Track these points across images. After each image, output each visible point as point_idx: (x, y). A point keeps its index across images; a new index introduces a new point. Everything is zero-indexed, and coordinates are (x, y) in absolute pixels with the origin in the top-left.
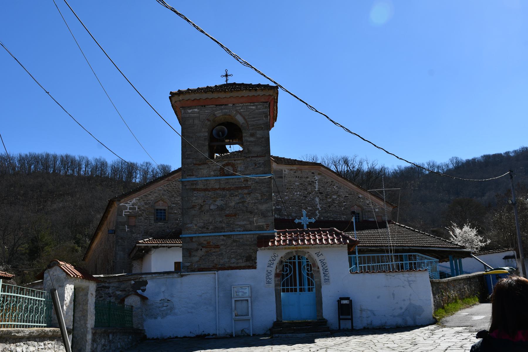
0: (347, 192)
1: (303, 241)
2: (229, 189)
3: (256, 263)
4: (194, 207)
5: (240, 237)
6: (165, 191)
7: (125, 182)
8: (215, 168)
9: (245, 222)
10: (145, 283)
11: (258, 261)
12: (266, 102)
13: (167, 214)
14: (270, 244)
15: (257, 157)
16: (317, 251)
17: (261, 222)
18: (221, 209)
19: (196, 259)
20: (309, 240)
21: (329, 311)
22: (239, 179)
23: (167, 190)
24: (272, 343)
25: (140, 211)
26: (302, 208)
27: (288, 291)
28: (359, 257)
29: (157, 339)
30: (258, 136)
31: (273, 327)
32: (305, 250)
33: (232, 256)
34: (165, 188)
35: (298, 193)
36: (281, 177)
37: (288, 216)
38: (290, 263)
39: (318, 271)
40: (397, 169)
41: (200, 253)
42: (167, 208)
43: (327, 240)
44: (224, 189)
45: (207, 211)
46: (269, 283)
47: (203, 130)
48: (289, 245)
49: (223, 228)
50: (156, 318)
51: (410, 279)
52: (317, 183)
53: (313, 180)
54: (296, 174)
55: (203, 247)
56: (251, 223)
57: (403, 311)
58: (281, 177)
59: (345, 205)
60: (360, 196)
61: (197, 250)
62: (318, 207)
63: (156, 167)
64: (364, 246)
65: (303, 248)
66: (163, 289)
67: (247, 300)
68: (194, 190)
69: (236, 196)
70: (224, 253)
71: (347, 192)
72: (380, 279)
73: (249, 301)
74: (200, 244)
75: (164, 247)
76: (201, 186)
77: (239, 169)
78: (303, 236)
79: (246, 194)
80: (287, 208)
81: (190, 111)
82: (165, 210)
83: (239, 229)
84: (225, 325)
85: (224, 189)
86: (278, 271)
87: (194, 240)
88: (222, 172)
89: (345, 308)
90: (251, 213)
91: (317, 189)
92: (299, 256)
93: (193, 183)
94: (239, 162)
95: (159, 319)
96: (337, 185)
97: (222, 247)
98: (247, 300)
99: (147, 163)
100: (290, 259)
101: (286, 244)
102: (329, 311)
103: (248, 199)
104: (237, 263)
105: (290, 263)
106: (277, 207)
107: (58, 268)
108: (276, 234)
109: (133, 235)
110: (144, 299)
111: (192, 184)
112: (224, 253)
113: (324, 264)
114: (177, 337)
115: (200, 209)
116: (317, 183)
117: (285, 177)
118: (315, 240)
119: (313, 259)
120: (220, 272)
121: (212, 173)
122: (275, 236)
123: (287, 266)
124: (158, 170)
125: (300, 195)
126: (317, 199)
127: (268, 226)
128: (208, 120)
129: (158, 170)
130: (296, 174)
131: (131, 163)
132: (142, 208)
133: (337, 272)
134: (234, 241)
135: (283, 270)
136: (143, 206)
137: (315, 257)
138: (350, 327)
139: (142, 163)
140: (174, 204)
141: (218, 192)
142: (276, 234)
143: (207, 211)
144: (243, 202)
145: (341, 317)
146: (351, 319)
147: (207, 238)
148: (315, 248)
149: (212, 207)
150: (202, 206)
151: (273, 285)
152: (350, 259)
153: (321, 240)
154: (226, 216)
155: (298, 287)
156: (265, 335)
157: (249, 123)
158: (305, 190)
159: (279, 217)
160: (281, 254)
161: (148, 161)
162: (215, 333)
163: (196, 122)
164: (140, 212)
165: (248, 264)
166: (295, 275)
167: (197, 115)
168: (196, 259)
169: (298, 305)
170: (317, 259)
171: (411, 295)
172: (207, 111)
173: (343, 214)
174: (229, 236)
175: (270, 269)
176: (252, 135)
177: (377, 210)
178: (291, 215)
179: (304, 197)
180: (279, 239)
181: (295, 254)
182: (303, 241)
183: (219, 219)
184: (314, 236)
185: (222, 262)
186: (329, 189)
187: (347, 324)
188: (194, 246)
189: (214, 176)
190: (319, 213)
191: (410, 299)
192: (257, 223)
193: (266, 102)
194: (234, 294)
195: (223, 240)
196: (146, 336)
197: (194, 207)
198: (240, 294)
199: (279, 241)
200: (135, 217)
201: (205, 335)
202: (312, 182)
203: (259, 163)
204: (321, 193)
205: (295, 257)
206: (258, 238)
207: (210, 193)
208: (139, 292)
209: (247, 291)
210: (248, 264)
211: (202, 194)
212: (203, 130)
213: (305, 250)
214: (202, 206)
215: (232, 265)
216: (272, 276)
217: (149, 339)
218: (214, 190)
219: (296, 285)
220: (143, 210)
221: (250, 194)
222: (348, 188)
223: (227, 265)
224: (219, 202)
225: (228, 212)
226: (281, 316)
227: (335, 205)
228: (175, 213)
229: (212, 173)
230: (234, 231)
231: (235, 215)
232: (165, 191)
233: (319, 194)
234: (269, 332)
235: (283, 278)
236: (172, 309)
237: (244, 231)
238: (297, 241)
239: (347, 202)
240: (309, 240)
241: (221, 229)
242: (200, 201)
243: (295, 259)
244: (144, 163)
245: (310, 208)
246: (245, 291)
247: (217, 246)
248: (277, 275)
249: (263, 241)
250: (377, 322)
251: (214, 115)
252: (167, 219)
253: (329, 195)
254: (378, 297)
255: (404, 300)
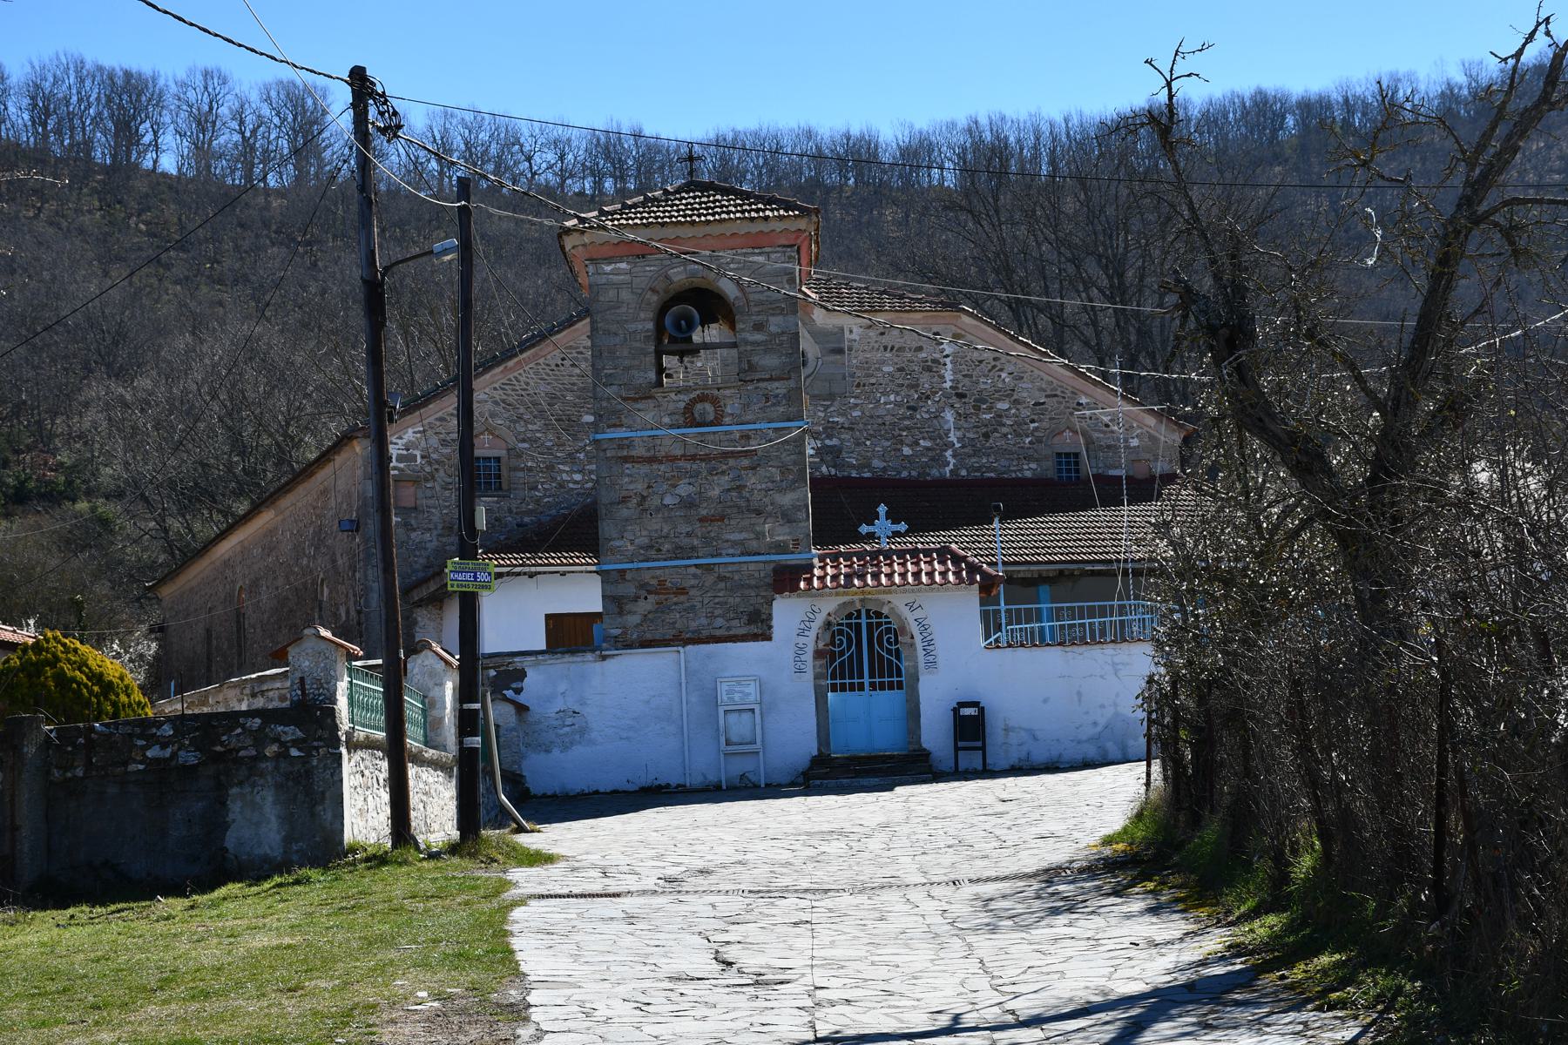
0: (1041, 390)
1: (876, 576)
2: (706, 458)
3: (770, 627)
4: (624, 500)
5: (735, 568)
6: (496, 403)
7: (105, 169)
8: (671, 407)
9: (744, 535)
10: (521, 675)
11: (774, 623)
12: (792, 246)
13: (504, 472)
14: (802, 585)
15: (771, 379)
16: (909, 598)
17: (783, 535)
18: (688, 504)
19: (633, 619)
20: (890, 576)
21: (935, 733)
22: (731, 433)
23: (504, 401)
24: (808, 792)
25: (430, 463)
26: (902, 442)
27: (843, 689)
28: (1007, 611)
29: (554, 796)
30: (773, 329)
31: (811, 768)
32: (881, 597)
33: (717, 612)
34: (498, 395)
35: (892, 397)
36: (840, 351)
37: (859, 468)
38: (849, 626)
39: (912, 645)
40: (1460, 78)
41: (644, 606)
42: (504, 452)
43: (930, 574)
44: (693, 458)
45: (658, 510)
46: (800, 671)
47: (642, 315)
48: (845, 587)
49: (693, 548)
50: (548, 751)
51: (1116, 660)
52: (949, 366)
53: (937, 356)
54: (885, 340)
55: (650, 592)
56: (759, 536)
57: (1099, 729)
58: (840, 351)
59: (1036, 429)
60: (1084, 400)
61: (636, 599)
62: (953, 438)
63: (254, 97)
64: (1073, 562)
65: (879, 592)
66: (562, 687)
67: (753, 710)
68: (626, 459)
69: (723, 473)
70: (699, 605)
71: (1041, 390)
72: (1051, 659)
73: (757, 712)
74: (643, 586)
75: (519, 574)
76: (639, 451)
77: (729, 410)
78: (877, 565)
79: (745, 469)
80: (858, 444)
81: (608, 268)
82: (498, 459)
83: (731, 551)
84: (704, 764)
85: (693, 458)
86: (821, 645)
87: (628, 576)
88: (690, 418)
89: (970, 726)
90: (759, 513)
91: (948, 385)
92: (868, 611)
93: (623, 444)
94: (728, 392)
95: (556, 752)
96: (1011, 368)
97: (692, 592)
98: (753, 710)
99: (207, 74)
100: (849, 616)
101: (839, 585)
102: (935, 733)
103: (751, 480)
104: (729, 629)
105: (849, 626)
106: (828, 442)
107: (430, 654)
108: (816, 561)
109: (413, 535)
110: (521, 709)
111: (620, 447)
112: (699, 605)
113: (924, 628)
114: (597, 792)
115: (639, 504)
116: (949, 366)
117: (850, 349)
118: (903, 575)
119: (899, 617)
120: (689, 647)
121: (666, 420)
122: (812, 566)
123: (841, 632)
124: (266, 111)
125: (896, 404)
126: (949, 416)
127: (797, 542)
128: (653, 290)
129: (266, 111)
130: (885, 340)
131: (128, 75)
132: (434, 456)
133: (956, 650)
134: (721, 578)
135: (833, 643)
136: (436, 450)
137: (905, 612)
138: (980, 768)
139: (182, 75)
140: (524, 441)
141: (681, 464)
142: (816, 561)
143: (658, 510)
144: (740, 488)
145: (960, 744)
146: (983, 749)
147: (658, 572)
148: (905, 592)
149: (668, 500)
150: (644, 498)
151: (809, 676)
152: (985, 616)
153: (917, 575)
154: (700, 520)
155: (866, 680)
156: (792, 784)
157: (751, 297)
158: (911, 386)
159: (833, 471)
160: (828, 606)
161: (210, 63)
162: (681, 782)
163: (625, 295)
164: (428, 469)
165: (754, 629)
166: (865, 652)
167: (627, 277)
168: (633, 619)
169: (867, 717)
170: (910, 617)
171: (1117, 695)
172: (650, 268)
173: (1029, 458)
174: (708, 568)
175: (802, 640)
176: (759, 327)
177: (1135, 443)
178: (868, 466)
179: (909, 408)
180: (823, 571)
181: (858, 606)
182: (876, 576)
183: (684, 528)
184: (904, 565)
185: (693, 625)
186: (985, 384)
187: (972, 760)
188: (629, 589)
189: (671, 427)
190: (954, 456)
191: (1115, 705)
192: (771, 536)
193: (792, 246)
194: (723, 696)
195: (695, 576)
196: (528, 789)
197: (624, 500)
198: (737, 697)
199: (822, 579)
200: (416, 481)
201: (660, 787)
202: (935, 361)
203: (776, 396)
204: (961, 396)
205: (859, 612)
206: (775, 571)
207: (662, 467)
208: (509, 693)
209: (752, 689)
210: (754, 629)
211: (644, 469)
212: (642, 315)
213: (881, 597)
214: (644, 498)
215: (718, 633)
216: (808, 656)
217: (535, 796)
218: (672, 459)
219: (861, 676)
220: (438, 462)
221: (754, 468)
222: (1046, 377)
223: (705, 633)
224: (684, 489)
225: (704, 512)
226: (828, 744)
227: (1005, 430)
228: (530, 469)
229: (666, 420)
230: (720, 555)
231: (722, 519)
232: (496, 403)
233: (954, 399)
234: (801, 780)
235: (833, 660)
236: (583, 731)
237: (742, 554)
238: (862, 577)
239: (1041, 421)
240: (890, 576)
241: (690, 552)
242: (639, 487)
243: (859, 617)
244: (191, 72)
245: (928, 444)
246: (747, 690)
247: (682, 591)
248: (818, 654)
249: (787, 579)
250: (1040, 756)
251: (667, 277)
252: (505, 486)
253: (985, 401)
254: (1045, 701)
255: (1102, 706)
